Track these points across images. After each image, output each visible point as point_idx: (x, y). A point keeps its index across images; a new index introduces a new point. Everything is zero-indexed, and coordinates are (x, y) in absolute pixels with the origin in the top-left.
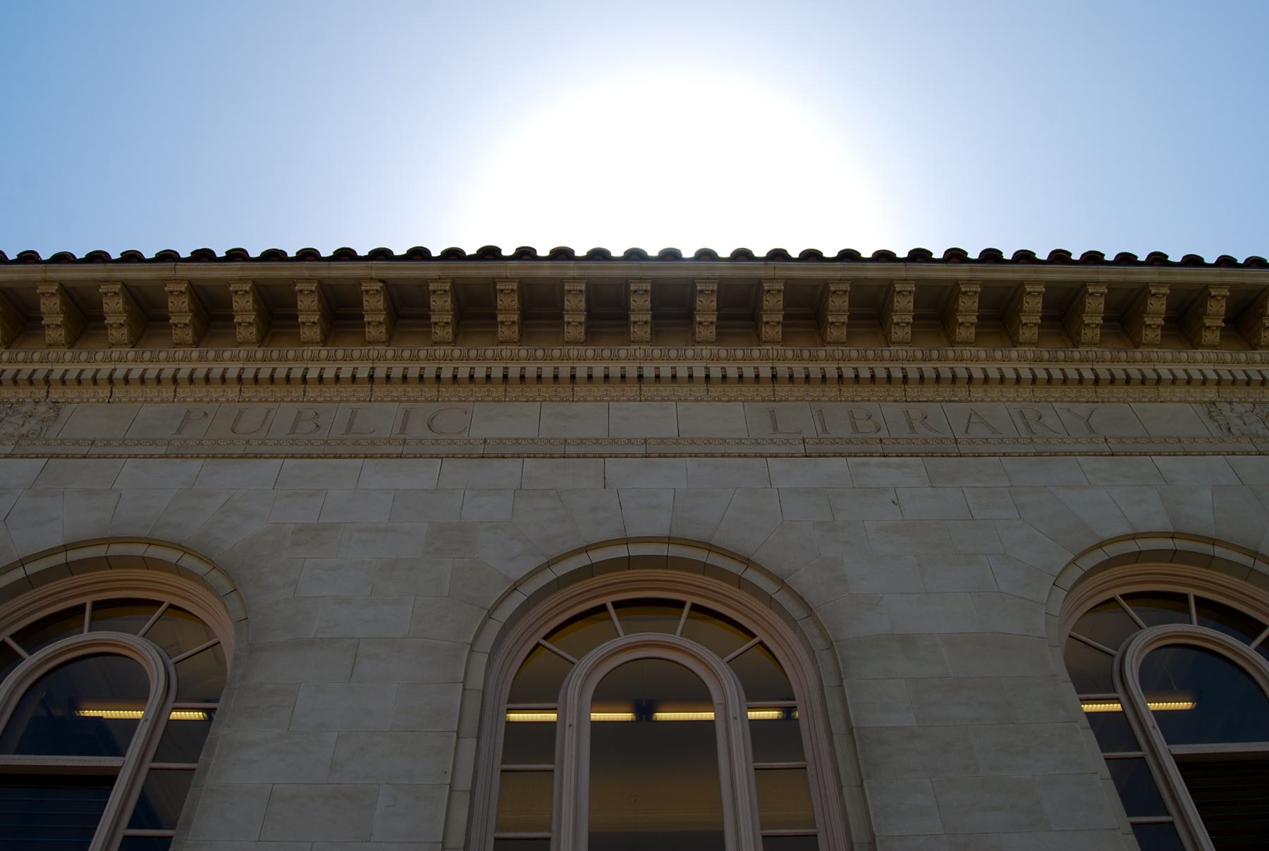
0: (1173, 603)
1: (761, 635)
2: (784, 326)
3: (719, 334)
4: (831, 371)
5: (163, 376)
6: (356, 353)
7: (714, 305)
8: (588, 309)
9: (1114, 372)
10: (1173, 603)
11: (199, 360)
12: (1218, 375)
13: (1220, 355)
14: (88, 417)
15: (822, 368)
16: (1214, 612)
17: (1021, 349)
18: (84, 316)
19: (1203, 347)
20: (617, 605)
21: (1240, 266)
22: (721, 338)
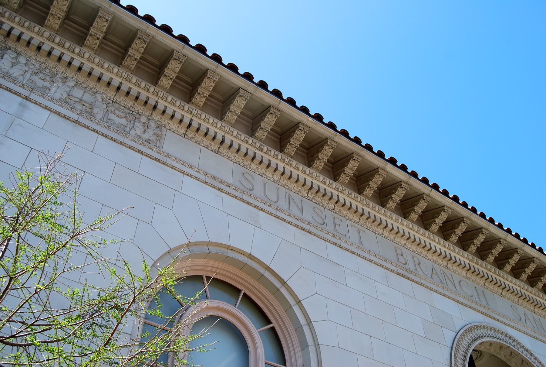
0: (231, 290)
1: (274, 324)
2: (174, 81)
3: (137, 67)
4: (116, 81)
5: (32, 42)
6: (67, 45)
7: (178, 70)
8: (106, 33)
9: (271, 162)
10: (231, 290)
11: (28, 29)
12: (357, 208)
13: (254, 143)
14: (174, 144)
15: (166, 107)
16: (250, 303)
17: (121, 70)
18: (189, 85)
19: (430, 231)
20: (245, 294)
21: (310, 115)
22: (204, 108)
